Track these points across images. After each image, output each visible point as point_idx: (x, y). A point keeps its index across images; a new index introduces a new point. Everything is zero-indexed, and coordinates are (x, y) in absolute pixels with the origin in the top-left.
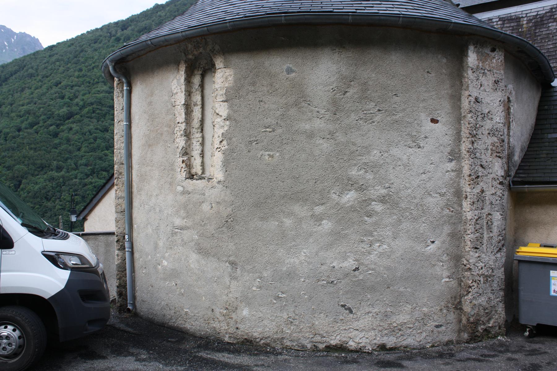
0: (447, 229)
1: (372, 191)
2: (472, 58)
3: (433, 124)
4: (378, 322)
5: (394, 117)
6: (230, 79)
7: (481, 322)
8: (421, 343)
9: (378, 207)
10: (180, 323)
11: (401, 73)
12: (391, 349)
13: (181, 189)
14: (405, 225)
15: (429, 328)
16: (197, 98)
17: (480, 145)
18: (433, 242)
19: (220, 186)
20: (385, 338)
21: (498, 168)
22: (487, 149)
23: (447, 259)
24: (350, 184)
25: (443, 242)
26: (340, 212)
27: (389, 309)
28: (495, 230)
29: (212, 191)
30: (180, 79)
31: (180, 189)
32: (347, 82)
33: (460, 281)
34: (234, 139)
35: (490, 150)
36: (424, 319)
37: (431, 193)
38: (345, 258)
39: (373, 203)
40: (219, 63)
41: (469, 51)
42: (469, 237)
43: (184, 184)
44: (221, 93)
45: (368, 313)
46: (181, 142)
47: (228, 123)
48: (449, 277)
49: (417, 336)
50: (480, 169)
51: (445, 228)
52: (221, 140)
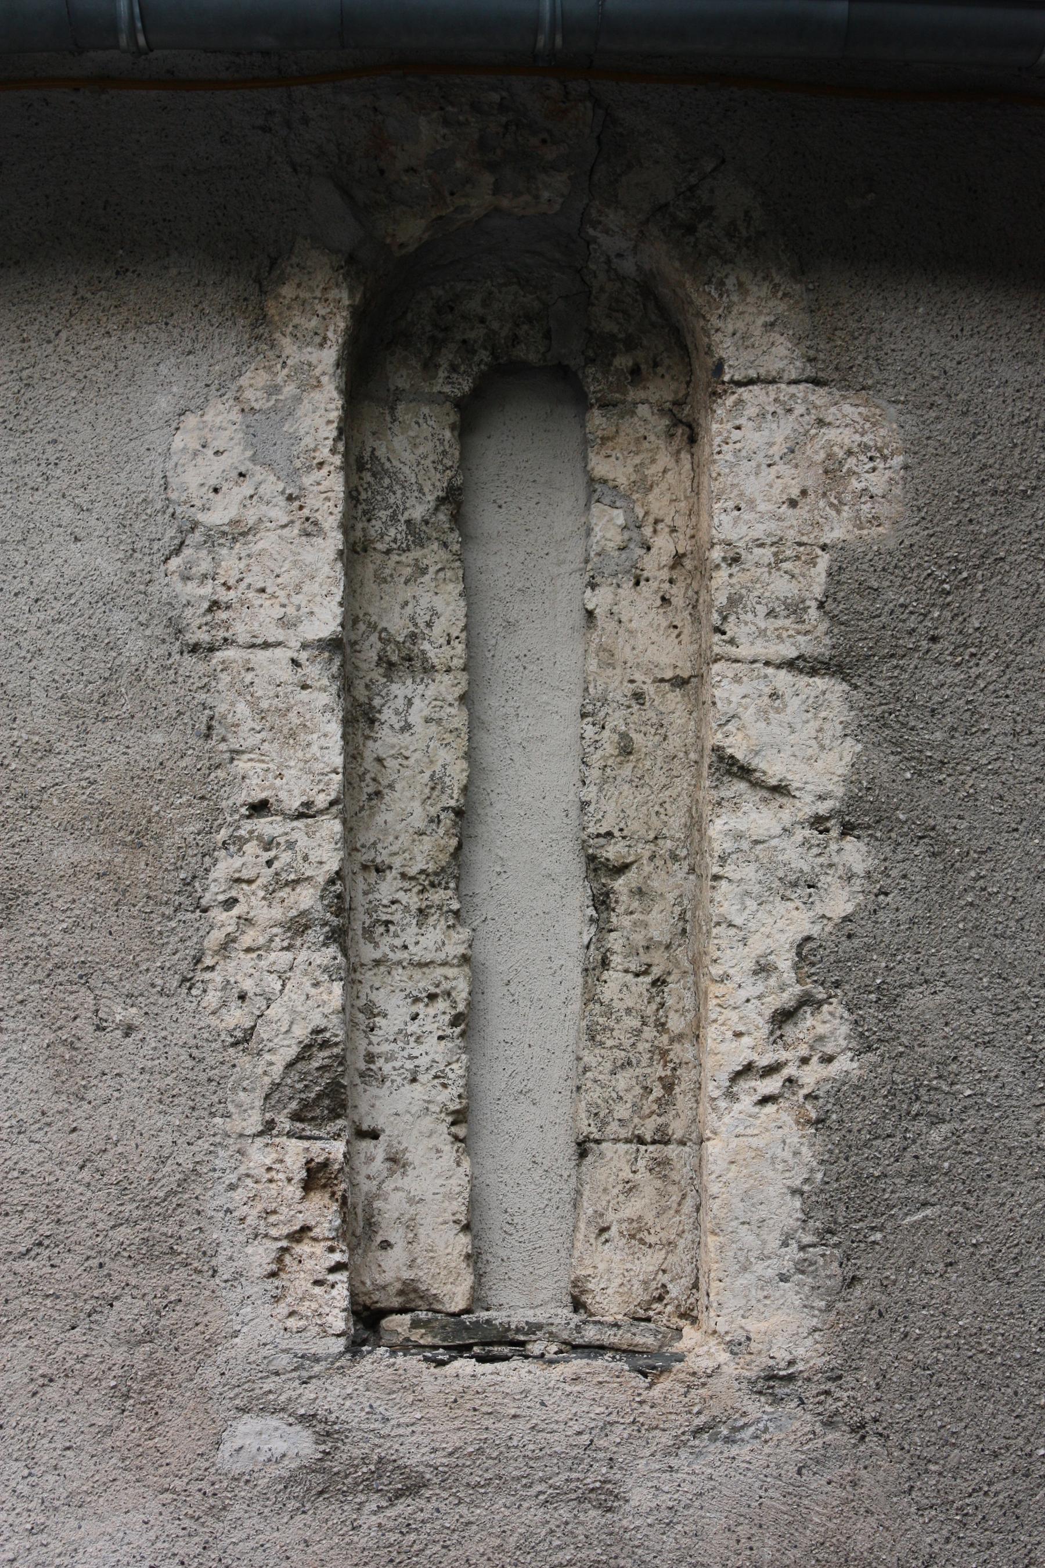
6: (877, 482)
13: (302, 1444)
19: (795, 1422)
29: (696, 1467)
30: (287, 412)
31: (269, 1442)
34: (920, 1001)
40: (750, 331)
43: (330, 1395)
44: (782, 587)
47: (854, 853)
52: (786, 999)
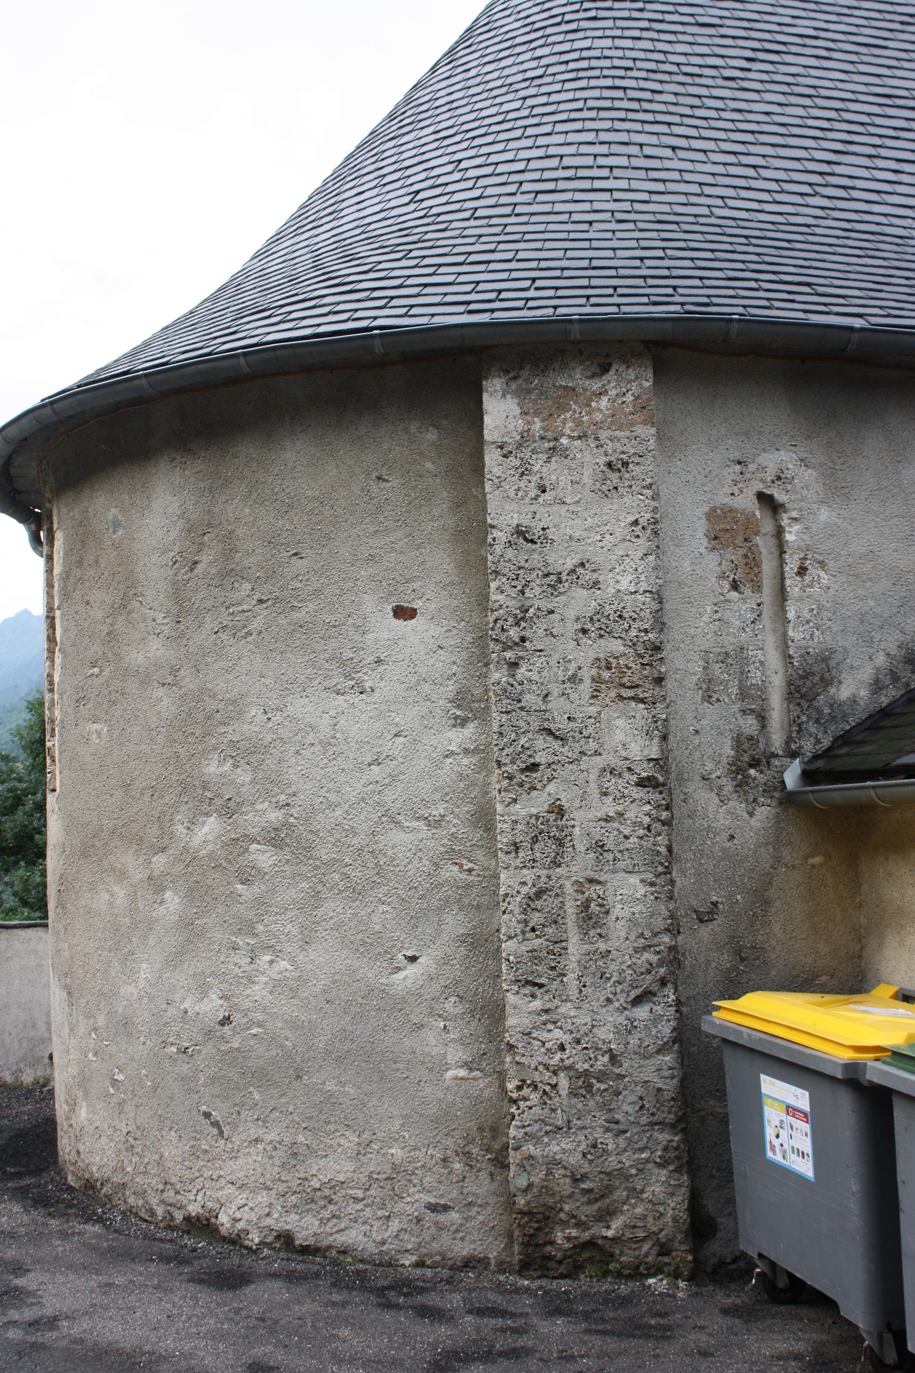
0: (455, 923)
1: (250, 816)
2: (501, 411)
3: (400, 623)
4: (277, 1169)
5: (295, 615)
7: (562, 1215)
8: (384, 1248)
9: (264, 857)
11: (309, 493)
12: (306, 1250)
14: (332, 908)
15: (410, 1209)
18: (413, 959)
20: (294, 1217)
22: (574, 679)
23: (460, 1009)
25: (445, 961)
26: (190, 869)
27: (301, 1138)
28: (619, 933)
32: (197, 531)
35: (588, 682)
36: (395, 1178)
37: (400, 818)
38: (203, 991)
39: (254, 847)
41: (485, 396)
45: (257, 1140)
48: (466, 1065)
49: (377, 1224)
50: (541, 742)
51: (449, 918)
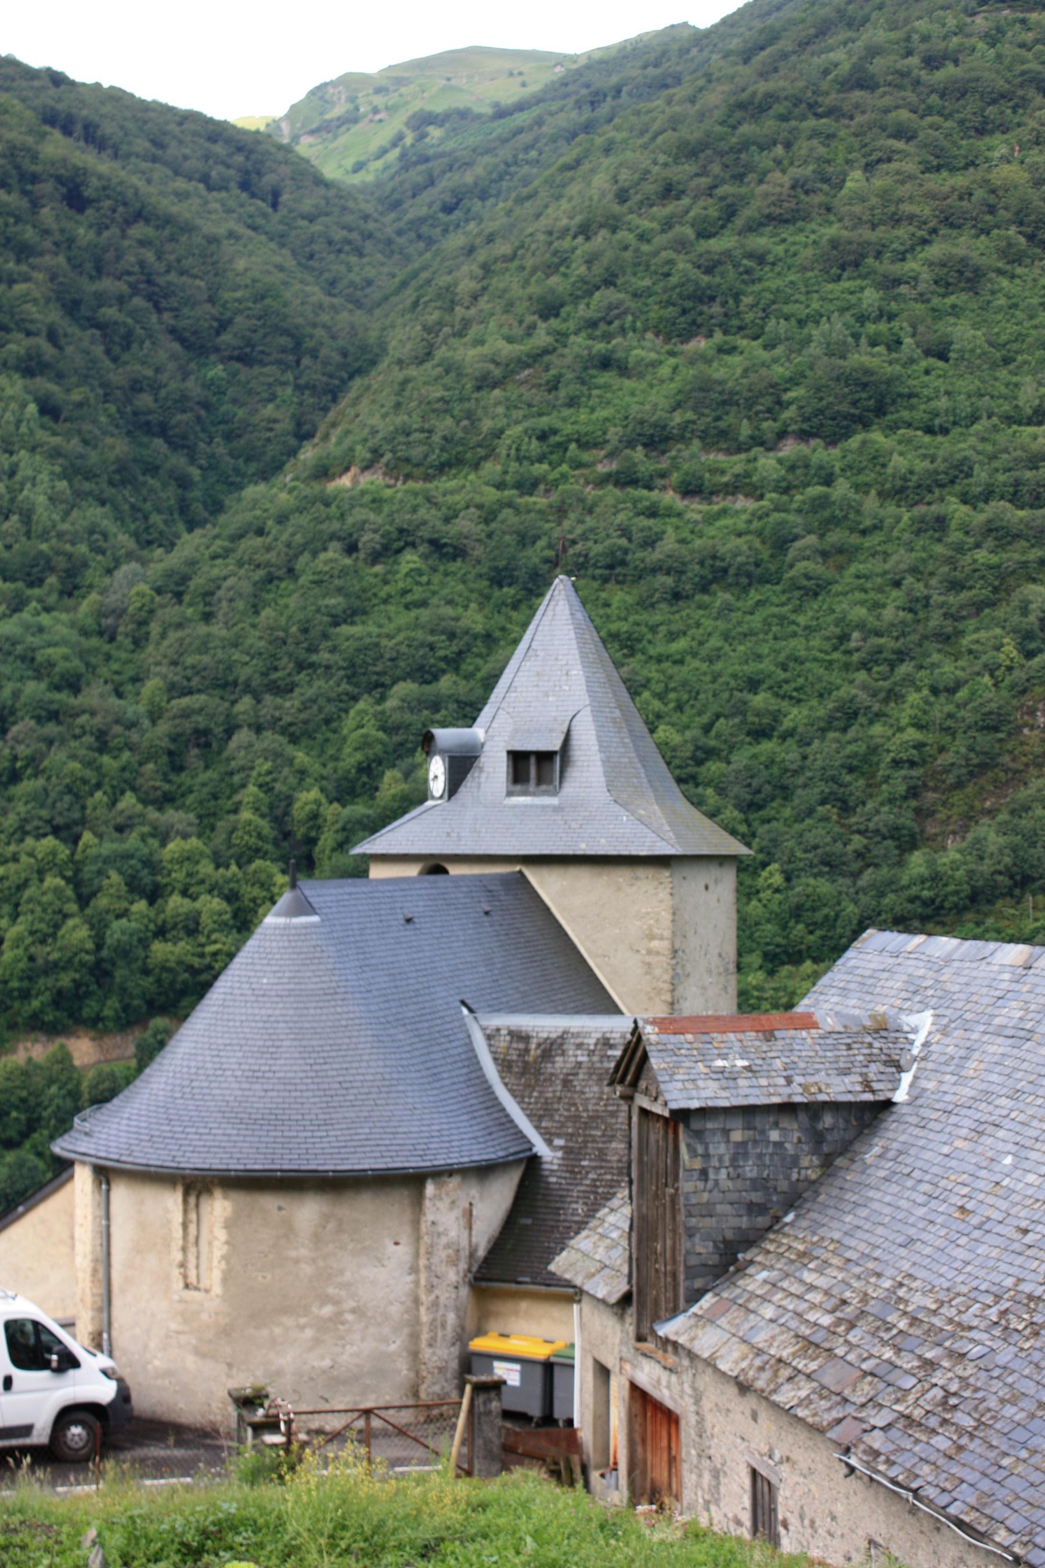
0: (406, 1331)
9: (349, 1317)
10: (173, 1417)
14: (372, 1330)
16: (193, 1216)
17: (435, 1260)
21: (453, 1275)
24: (326, 1299)
28: (449, 1328)
31: (176, 1297)
32: (326, 1218)
33: (417, 1373)
38: (323, 1358)
42: (425, 1336)
46: (178, 1256)
